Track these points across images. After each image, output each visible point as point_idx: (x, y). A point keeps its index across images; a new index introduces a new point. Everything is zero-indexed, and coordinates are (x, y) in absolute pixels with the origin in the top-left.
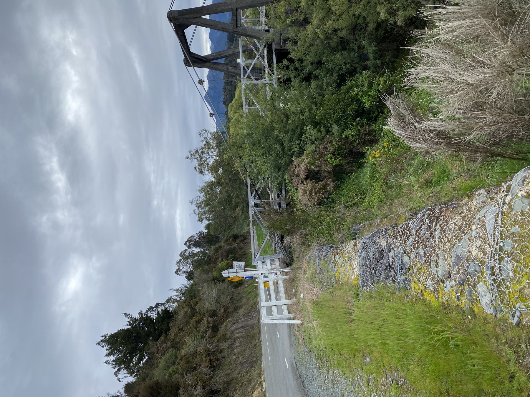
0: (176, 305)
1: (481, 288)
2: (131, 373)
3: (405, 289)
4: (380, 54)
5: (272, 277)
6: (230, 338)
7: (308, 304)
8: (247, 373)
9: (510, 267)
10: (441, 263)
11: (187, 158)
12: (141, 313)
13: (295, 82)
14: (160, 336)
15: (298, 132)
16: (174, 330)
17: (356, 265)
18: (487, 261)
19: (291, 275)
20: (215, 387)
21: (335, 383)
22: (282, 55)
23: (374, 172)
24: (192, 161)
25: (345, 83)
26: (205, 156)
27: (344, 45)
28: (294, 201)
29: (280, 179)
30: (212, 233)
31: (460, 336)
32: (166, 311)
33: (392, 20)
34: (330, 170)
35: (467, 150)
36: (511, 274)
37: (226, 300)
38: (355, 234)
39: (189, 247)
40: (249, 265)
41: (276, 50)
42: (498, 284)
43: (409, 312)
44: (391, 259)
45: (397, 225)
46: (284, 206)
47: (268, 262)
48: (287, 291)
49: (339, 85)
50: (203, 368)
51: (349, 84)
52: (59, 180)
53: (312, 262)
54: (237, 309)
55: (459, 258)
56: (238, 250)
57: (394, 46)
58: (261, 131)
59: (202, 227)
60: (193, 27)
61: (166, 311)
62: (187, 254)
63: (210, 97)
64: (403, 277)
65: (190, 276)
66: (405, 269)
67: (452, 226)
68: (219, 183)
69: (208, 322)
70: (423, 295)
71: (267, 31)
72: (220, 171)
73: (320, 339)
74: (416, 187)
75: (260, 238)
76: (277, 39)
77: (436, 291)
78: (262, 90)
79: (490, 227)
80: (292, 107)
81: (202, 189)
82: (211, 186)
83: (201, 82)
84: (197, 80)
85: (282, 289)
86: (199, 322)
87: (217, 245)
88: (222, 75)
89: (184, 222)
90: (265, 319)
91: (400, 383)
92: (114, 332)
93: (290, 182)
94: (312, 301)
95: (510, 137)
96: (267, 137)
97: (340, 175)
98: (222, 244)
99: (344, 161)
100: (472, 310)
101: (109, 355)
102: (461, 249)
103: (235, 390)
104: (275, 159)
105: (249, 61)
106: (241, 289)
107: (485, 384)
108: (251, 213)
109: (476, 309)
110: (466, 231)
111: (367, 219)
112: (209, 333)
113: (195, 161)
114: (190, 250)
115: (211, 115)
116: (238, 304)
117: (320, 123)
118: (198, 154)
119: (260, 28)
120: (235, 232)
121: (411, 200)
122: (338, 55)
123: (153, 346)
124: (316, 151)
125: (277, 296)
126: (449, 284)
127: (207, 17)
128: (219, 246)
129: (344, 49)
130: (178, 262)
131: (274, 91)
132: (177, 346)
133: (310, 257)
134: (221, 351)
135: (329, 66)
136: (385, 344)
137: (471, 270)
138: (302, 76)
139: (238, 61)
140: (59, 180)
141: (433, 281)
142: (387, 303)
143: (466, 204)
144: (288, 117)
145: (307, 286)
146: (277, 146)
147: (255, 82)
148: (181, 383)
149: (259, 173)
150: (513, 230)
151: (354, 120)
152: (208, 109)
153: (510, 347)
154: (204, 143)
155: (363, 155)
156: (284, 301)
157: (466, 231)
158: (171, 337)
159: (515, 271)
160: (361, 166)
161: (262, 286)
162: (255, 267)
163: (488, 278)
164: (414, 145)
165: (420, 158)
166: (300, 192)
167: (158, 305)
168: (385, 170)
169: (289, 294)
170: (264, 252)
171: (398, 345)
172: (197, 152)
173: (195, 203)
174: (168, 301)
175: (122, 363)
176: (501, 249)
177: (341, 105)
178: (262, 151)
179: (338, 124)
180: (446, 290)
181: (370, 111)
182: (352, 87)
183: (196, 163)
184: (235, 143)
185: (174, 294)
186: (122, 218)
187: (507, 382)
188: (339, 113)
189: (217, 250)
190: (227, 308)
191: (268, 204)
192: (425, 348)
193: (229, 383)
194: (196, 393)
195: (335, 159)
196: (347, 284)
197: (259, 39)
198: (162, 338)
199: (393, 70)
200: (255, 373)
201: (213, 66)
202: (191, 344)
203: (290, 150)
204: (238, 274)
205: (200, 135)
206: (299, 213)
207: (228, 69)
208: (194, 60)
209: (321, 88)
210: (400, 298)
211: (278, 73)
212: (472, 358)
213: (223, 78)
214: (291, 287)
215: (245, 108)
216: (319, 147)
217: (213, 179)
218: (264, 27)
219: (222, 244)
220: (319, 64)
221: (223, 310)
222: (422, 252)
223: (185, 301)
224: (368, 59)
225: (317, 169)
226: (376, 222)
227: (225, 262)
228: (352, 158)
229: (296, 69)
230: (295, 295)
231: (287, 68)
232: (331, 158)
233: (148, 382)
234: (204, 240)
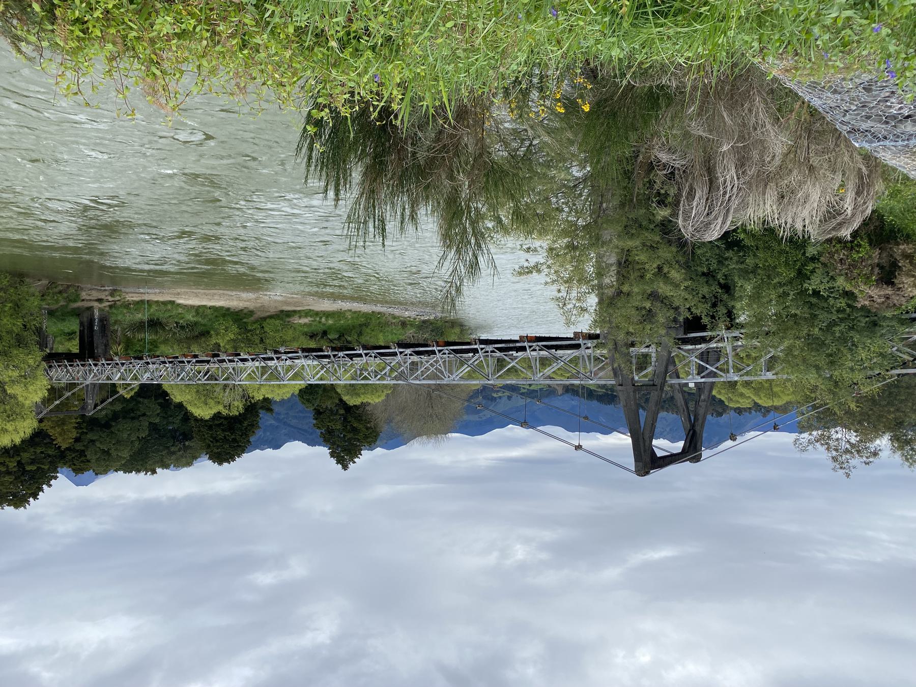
11: (848, 475)
15: (814, 300)
22: (694, 324)
24: (854, 467)
25: (740, 241)
34: (878, 251)
41: (685, 333)
58: (813, 354)
76: (673, 334)
81: (907, 460)
93: (899, 308)
113: (853, 462)
117: (800, 272)
119: (654, 355)
124: (846, 274)
146: (837, 329)
154: (818, 445)
172: (835, 459)
183: (856, 461)
195: (859, 246)
201: (700, 421)
205: (804, 450)
207: (704, 401)
213: (675, 415)
216: (841, 270)
225: (877, 270)
232: (858, 252)
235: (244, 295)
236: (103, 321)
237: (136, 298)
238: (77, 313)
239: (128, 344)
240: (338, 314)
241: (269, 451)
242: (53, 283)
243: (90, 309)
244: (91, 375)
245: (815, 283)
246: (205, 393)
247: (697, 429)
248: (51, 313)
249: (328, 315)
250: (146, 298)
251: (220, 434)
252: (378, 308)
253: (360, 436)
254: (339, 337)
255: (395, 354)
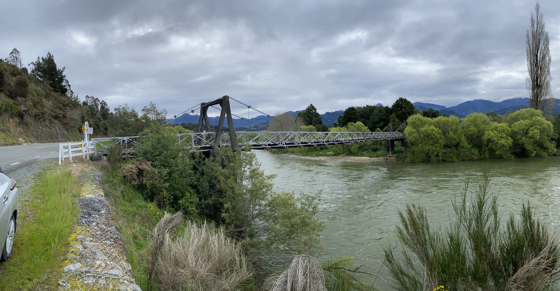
0: (70, 96)
1: (78, 265)
2: (33, 71)
3: (78, 223)
4: (208, 206)
5: (84, 149)
6: (51, 126)
7: (69, 169)
8: (32, 135)
9: (90, 282)
10: (92, 244)
11: (151, 102)
12: (65, 76)
13: (193, 162)
14: (52, 87)
15: (166, 164)
16: (56, 94)
17: (91, 196)
18: (93, 269)
19: (85, 160)
20: (25, 117)
21: (27, 183)
23: (142, 207)
26: (152, 112)
27: (212, 187)
28: (126, 162)
29: (139, 154)
30: (109, 116)
31: (52, 252)
32: (66, 90)
33: (224, 211)
35: (153, 259)
36: (86, 282)
37: (72, 124)
38: (108, 196)
39: (101, 103)
40: (91, 136)
42: (80, 275)
43: (65, 224)
44: (94, 215)
45: (113, 219)
46: (123, 156)
47: (93, 147)
48: (76, 157)
49: (191, 186)
50: (35, 111)
51: (192, 191)
52: (140, 31)
53: (92, 171)
54: (67, 129)
55: (95, 253)
56: (100, 130)
57: (212, 213)
59: (112, 111)
60: (221, 108)
61: (66, 90)
62: (97, 102)
63: (186, 116)
64: (84, 222)
65: (85, 103)
66: (89, 223)
67: (112, 250)
68: (137, 120)
69: (60, 114)
70: (75, 232)
71: (219, 147)
72: (144, 121)
73: (51, 175)
74: (133, 231)
75: (106, 143)
76: (215, 151)
77: (76, 240)
78: (189, 144)
79: (111, 272)
80: (179, 161)
82: (135, 116)
83: (193, 111)
84: (193, 109)
85: (78, 154)
86: (60, 108)
87: (102, 119)
88: (197, 123)
89: (115, 100)
90: (61, 145)
91: (27, 218)
92: (55, 61)
94: (71, 171)
95: (160, 282)
96: (163, 147)
97: (141, 188)
98: (103, 122)
99: (148, 190)
100: (66, 259)
101: (43, 59)
102: (99, 255)
103: (23, 128)
104: (150, 151)
105: (204, 137)
106: (77, 132)
107: (26, 264)
108: (120, 138)
109: (67, 261)
110: (110, 258)
111: (115, 203)
112: (54, 114)
114: (99, 104)
115: (175, 116)
116: (69, 130)
117: (171, 176)
118: (153, 109)
120: (109, 129)
121: (126, 228)
122: (207, 184)
123: (47, 83)
125: (74, 151)
126: (80, 248)
127: (226, 116)
128: (102, 120)
129: (210, 187)
130: (93, 98)
131: (188, 150)
132: (47, 96)
133: (95, 171)
134: (44, 121)
135: (201, 180)
136: (48, 211)
137: (88, 260)
138: (196, 165)
139: (204, 131)
140: (140, 31)
141: (82, 239)
142: (70, 213)
143: (123, 258)
144: (174, 158)
145: (80, 168)
146: (157, 153)
147: (193, 140)
148: (28, 99)
149: (142, 143)
150: (110, 284)
151: (172, 195)
152: (179, 115)
153: (46, 279)
155: (152, 200)
156: (71, 155)
157: (110, 258)
158: (52, 93)
159: (88, 284)
160: (146, 199)
161: (79, 143)
162: (90, 140)
163: (84, 269)
164: (156, 229)
165: (150, 233)
166: (131, 166)
167: (69, 86)
168: (143, 213)
169: (75, 158)
170: (98, 145)
171: (47, 218)
172: (155, 108)
173: (126, 106)
174: (71, 91)
175: (39, 67)
176: (100, 277)
177: (180, 187)
178: (155, 145)
179: (170, 186)
180: (77, 246)
181: (177, 203)
182: (190, 192)
184: (159, 129)
185: (75, 95)
186: (117, 66)
187: (28, 277)
188: (176, 186)
189: (99, 119)
190: (67, 124)
191: (125, 148)
192: (46, 232)
193: (27, 125)
194: (22, 107)
196: (81, 191)
197: (215, 142)
198: (52, 88)
199: (200, 214)
200: (32, 139)
202: (48, 104)
203: (155, 160)
204: (86, 131)
206: (119, 165)
208: (204, 108)
209: (190, 176)
210: (72, 220)
211: (197, 152)
212: (40, 258)
214: (79, 160)
215: (179, 135)
217: (139, 117)
218: (221, 144)
219: (103, 122)
220: (203, 174)
221: (67, 122)
222: (98, 233)
223: (71, 101)
224: (205, 200)
225: (144, 175)
226: (114, 208)
227: (92, 123)
228: (151, 196)
229: (200, 162)
230: (74, 162)
231: (200, 157)
233: (28, 80)
234: (105, 112)
235: (350, 161)
236: (388, 151)
237: (380, 158)
238: (395, 153)
239: (381, 144)
240: (318, 155)
241: (330, 111)
242: (403, 161)
243: (392, 154)
244: (396, 135)
245: (165, 171)
246: (359, 129)
247: (202, 115)
248: (402, 152)
249: (322, 155)
250: (378, 158)
251: (353, 116)
252: (304, 158)
253: (307, 115)
254: (318, 148)
255: (315, 142)
